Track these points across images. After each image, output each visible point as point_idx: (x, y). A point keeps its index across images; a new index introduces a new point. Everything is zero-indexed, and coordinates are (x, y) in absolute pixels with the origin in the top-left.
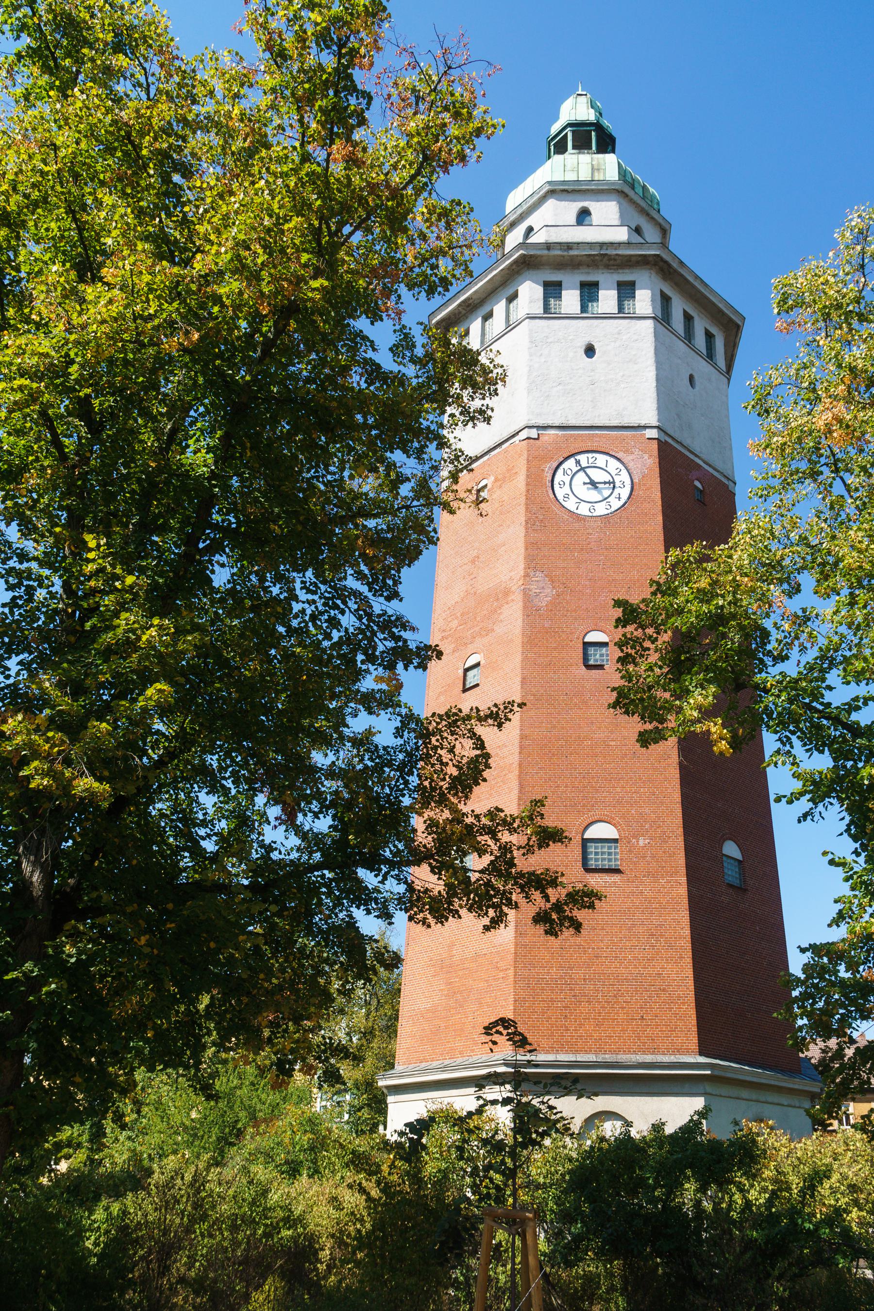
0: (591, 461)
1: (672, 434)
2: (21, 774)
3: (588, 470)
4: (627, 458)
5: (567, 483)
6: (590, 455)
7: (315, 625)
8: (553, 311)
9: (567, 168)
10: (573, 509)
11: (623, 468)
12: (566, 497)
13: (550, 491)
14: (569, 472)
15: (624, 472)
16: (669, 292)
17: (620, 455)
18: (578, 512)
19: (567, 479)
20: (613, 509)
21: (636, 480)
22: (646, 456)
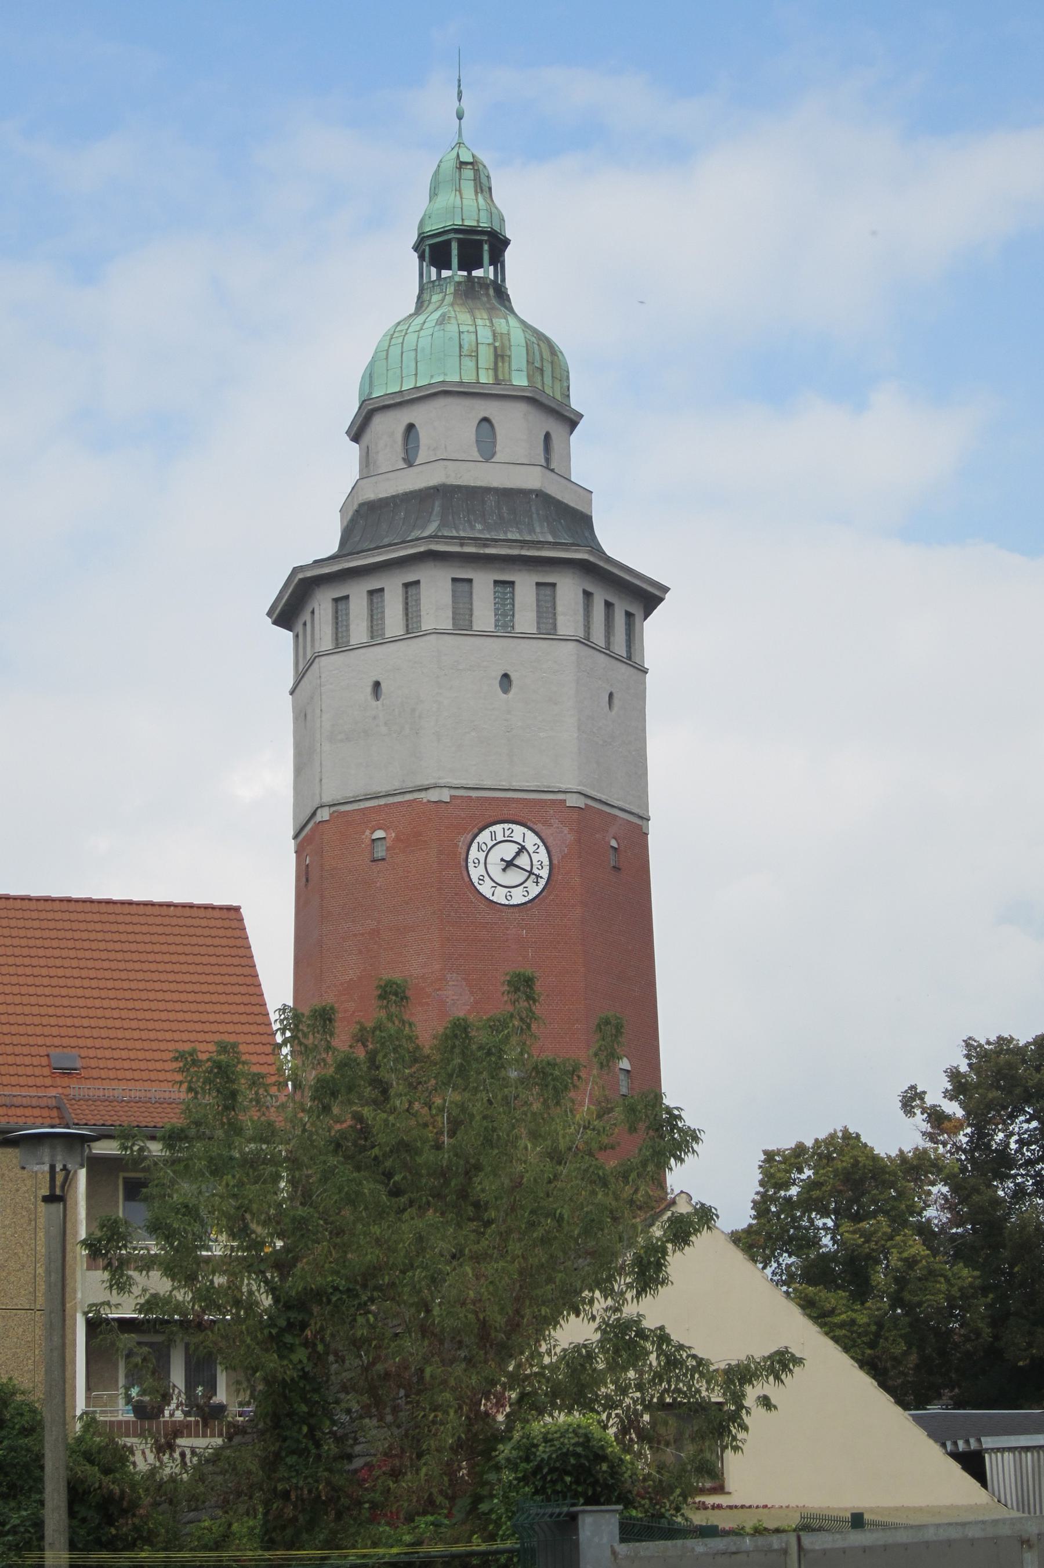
0: (507, 833)
1: (424, 638)
2: (219, 1441)
3: (529, 869)
4: (545, 832)
5: (482, 861)
6: (506, 826)
7: (670, 1386)
8: (475, 628)
9: (465, 352)
10: (489, 895)
11: (541, 844)
12: (481, 879)
13: (465, 874)
14: (484, 847)
15: (542, 849)
16: (590, 589)
17: (538, 827)
18: (494, 899)
19: (481, 856)
20: (530, 897)
21: (555, 862)
22: (566, 830)
